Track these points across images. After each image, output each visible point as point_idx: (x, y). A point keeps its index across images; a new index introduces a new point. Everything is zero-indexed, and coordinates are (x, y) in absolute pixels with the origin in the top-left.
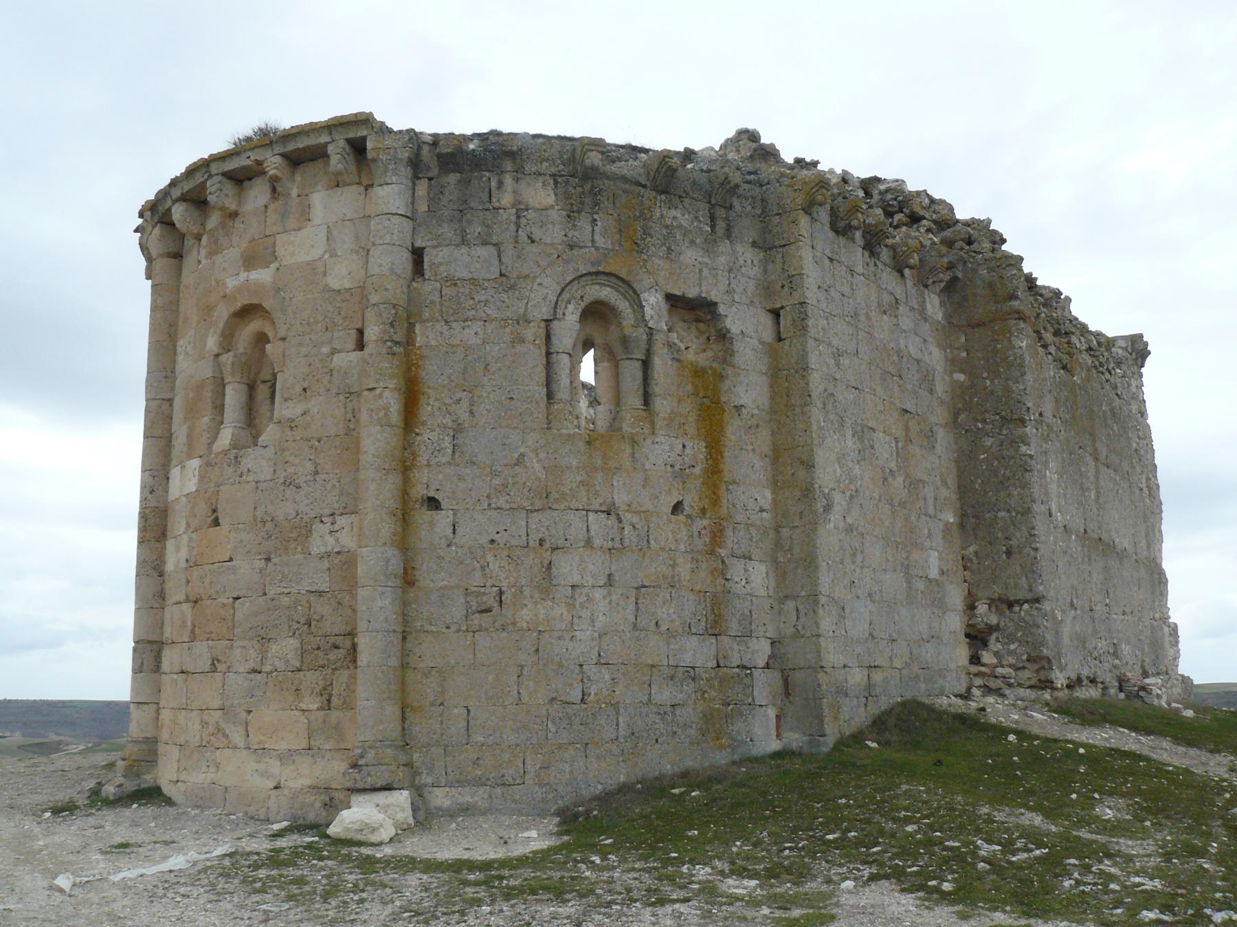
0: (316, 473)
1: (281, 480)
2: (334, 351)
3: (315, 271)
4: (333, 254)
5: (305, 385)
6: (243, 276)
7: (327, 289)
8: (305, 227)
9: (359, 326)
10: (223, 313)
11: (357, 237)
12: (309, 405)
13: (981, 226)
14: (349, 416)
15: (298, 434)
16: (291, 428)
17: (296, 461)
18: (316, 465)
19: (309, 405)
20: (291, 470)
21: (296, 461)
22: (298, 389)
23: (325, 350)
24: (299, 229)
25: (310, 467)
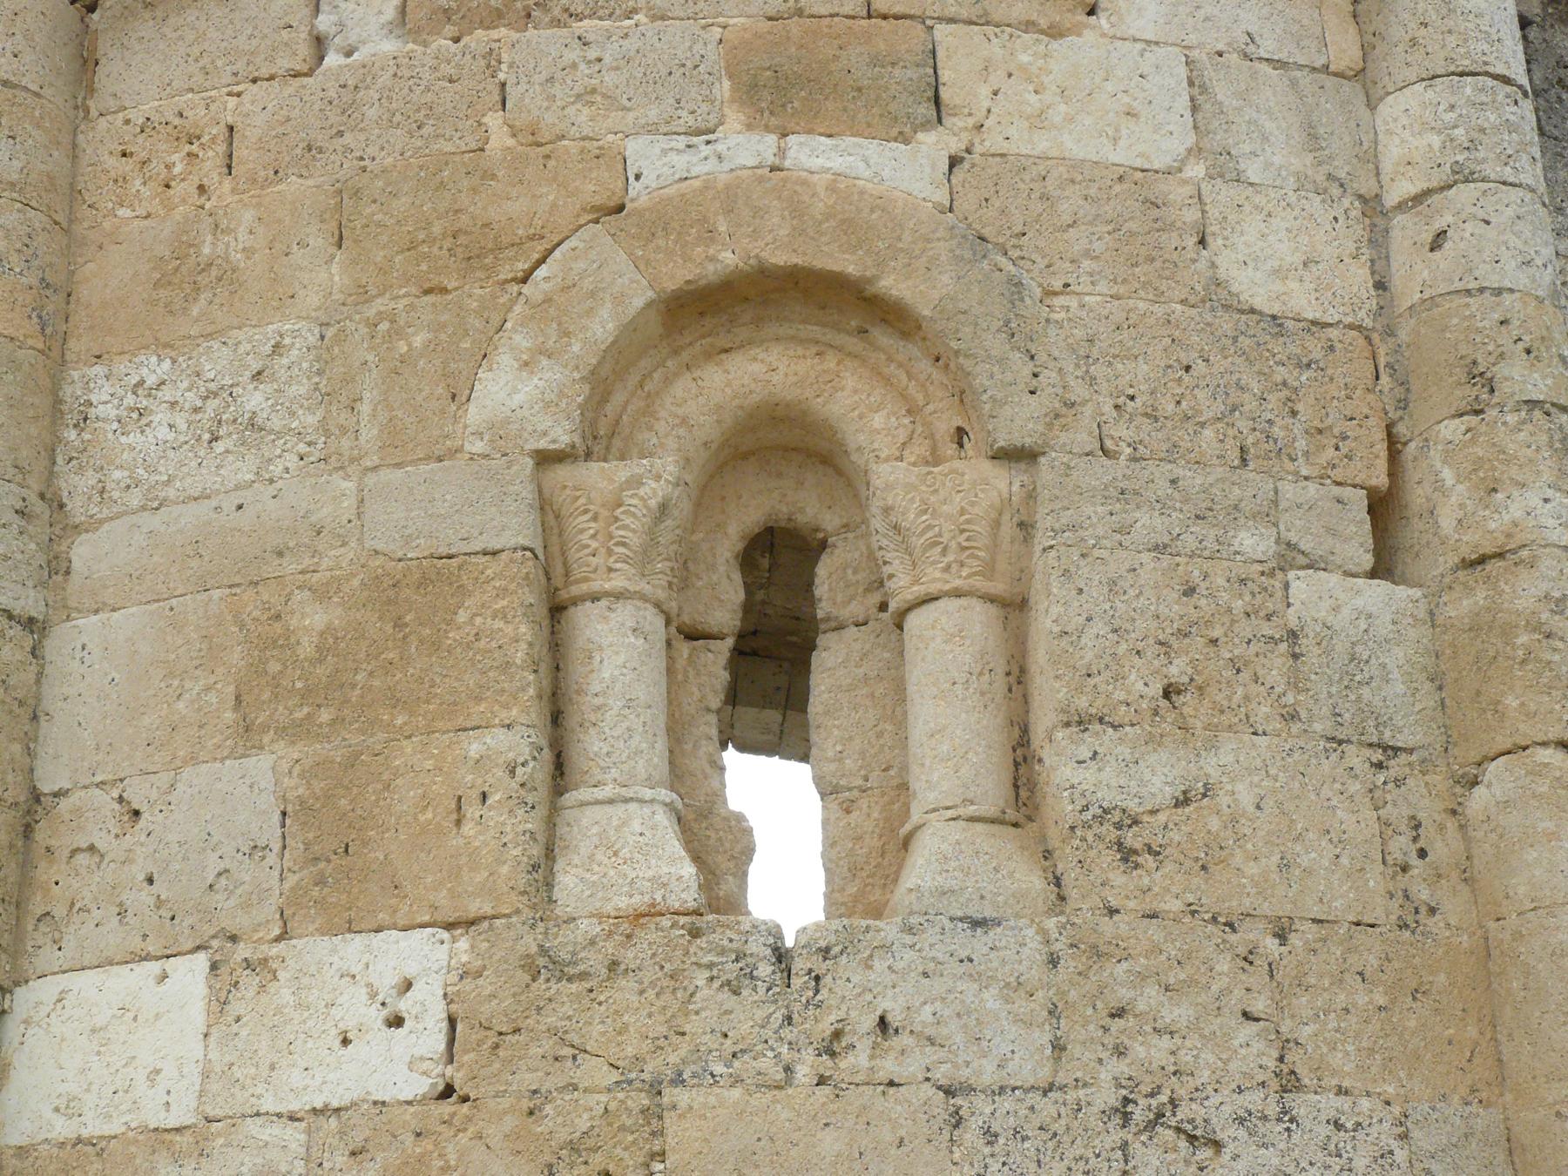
0: (1289, 1083)
1: (1108, 1097)
2: (1289, 557)
3: (1154, 225)
4: (1225, 169)
5: (1177, 670)
6: (744, 148)
7: (1215, 295)
8: (1076, 30)
9: (1380, 479)
10: (615, 285)
11: (1312, 139)
12: (1211, 766)
13: (740, 818)
14: (1401, 845)
15: (1168, 886)
16: (1127, 855)
17: (1177, 1013)
18: (1286, 1045)
19: (1211, 766)
20: (1157, 1051)
21: (1177, 1013)
22: (1142, 684)
23: (1253, 542)
24: (1055, 32)
25: (1252, 1051)
